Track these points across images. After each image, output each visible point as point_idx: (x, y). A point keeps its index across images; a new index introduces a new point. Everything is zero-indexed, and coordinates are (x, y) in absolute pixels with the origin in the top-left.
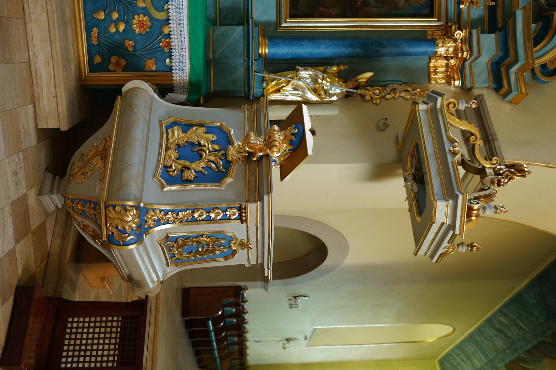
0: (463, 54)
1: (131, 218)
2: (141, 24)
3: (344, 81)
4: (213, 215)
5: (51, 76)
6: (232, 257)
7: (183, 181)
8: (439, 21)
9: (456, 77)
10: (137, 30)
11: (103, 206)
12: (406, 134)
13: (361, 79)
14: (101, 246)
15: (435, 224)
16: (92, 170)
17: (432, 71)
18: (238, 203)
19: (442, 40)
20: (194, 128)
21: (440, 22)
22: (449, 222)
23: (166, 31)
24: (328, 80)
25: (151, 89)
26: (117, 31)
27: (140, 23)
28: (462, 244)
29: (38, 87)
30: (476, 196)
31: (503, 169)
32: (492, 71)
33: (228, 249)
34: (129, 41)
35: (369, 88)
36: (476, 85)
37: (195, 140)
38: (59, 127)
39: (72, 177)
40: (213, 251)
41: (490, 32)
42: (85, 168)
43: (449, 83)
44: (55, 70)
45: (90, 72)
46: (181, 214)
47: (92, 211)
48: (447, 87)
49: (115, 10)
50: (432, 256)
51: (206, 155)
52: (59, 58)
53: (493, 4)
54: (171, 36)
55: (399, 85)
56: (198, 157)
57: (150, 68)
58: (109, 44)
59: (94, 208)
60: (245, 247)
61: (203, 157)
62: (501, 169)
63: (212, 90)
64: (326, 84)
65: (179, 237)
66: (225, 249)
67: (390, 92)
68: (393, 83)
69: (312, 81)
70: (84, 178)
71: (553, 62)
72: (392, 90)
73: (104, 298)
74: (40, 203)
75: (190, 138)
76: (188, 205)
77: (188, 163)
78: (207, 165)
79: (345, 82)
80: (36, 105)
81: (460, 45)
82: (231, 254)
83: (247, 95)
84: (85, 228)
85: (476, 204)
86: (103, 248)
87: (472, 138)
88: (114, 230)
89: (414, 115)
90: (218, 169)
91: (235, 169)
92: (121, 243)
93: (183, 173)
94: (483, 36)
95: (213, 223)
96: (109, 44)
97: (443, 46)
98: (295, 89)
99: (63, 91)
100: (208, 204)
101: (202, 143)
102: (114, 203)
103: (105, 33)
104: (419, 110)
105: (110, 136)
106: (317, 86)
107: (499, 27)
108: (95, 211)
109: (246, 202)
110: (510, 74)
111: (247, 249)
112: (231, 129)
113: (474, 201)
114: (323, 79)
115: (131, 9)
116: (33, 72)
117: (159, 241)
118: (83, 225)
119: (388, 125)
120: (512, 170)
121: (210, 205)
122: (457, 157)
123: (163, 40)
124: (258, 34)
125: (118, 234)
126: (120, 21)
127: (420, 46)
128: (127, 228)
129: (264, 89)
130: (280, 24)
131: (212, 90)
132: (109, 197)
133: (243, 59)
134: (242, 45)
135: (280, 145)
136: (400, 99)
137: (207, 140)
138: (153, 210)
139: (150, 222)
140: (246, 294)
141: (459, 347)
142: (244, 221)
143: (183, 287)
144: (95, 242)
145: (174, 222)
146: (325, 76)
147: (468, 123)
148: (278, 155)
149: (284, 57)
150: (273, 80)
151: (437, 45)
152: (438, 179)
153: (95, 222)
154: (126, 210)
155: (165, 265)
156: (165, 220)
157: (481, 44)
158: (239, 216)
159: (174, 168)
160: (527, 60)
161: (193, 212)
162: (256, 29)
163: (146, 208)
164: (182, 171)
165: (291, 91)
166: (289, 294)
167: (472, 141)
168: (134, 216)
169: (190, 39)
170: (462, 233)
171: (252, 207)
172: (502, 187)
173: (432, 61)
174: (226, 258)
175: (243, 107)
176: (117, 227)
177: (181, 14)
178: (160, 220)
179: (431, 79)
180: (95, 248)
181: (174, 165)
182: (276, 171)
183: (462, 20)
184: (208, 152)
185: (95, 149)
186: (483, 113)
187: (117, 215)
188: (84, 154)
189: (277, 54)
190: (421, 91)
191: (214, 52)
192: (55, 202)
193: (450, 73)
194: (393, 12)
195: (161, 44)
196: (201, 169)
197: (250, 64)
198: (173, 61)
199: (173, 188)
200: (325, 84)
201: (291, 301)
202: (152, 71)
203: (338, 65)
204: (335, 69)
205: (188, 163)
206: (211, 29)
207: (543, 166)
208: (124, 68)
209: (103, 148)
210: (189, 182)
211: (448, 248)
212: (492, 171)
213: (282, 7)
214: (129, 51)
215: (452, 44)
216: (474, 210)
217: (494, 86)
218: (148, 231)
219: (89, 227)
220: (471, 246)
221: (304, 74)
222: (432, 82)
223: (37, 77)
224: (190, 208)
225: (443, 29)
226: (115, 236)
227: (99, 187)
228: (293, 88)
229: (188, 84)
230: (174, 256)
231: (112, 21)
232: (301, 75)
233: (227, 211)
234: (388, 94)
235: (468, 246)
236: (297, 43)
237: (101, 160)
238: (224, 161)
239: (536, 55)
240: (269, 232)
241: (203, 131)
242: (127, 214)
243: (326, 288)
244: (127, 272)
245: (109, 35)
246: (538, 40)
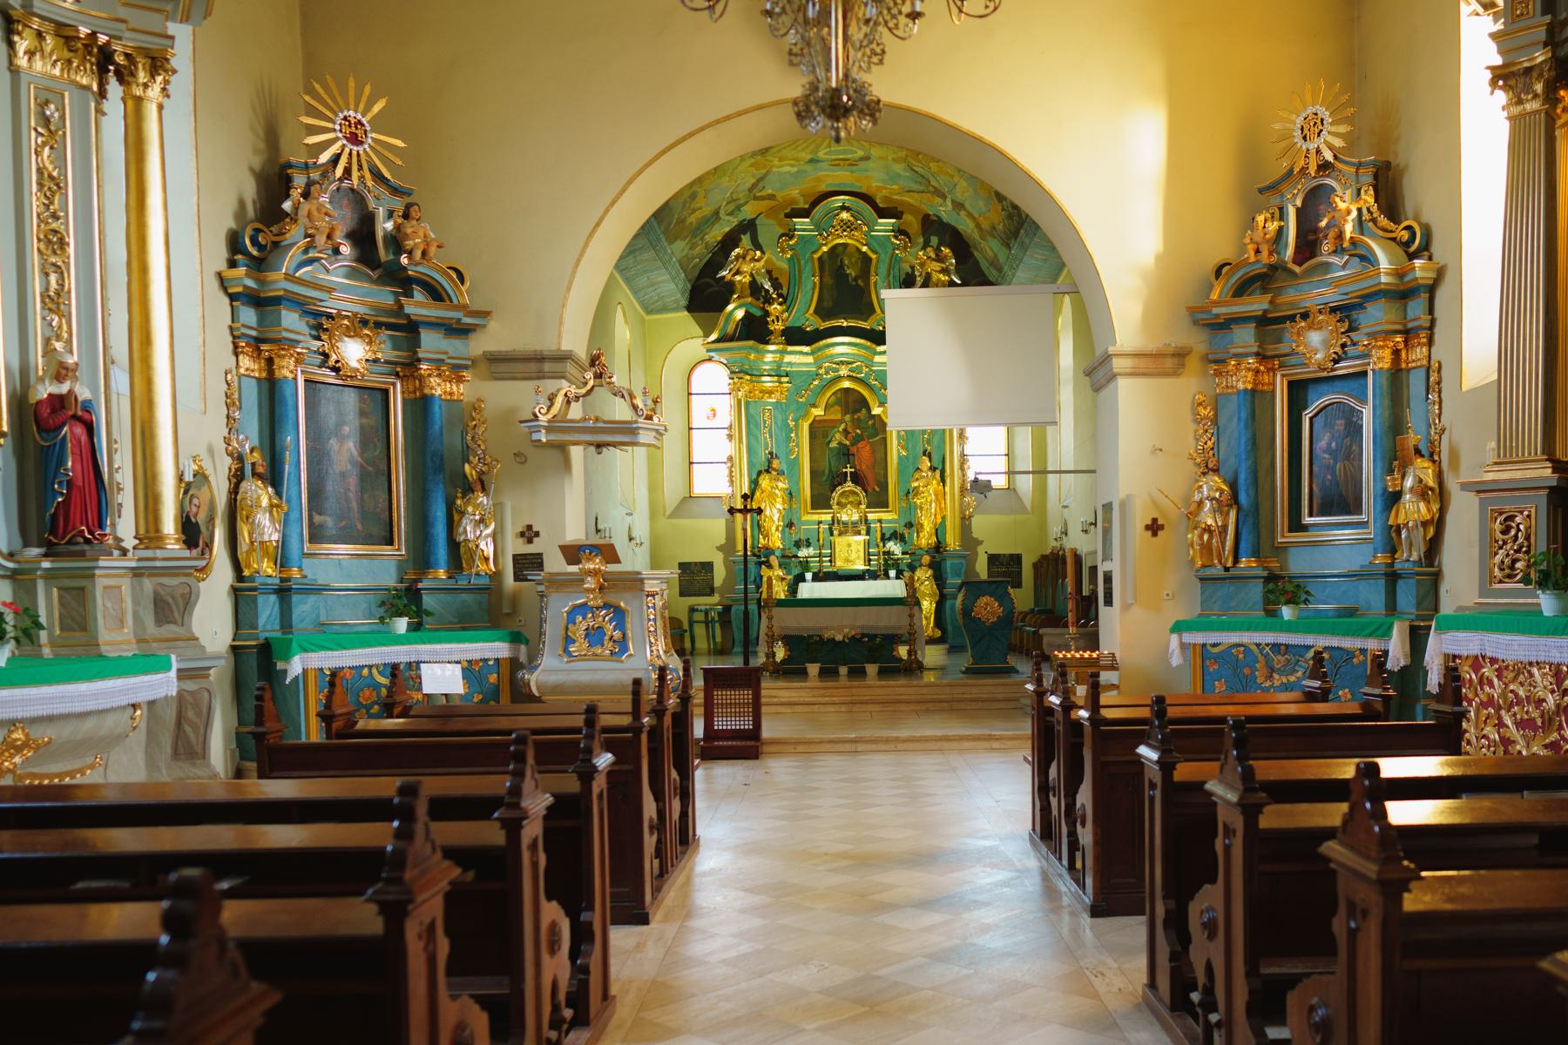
22: (654, 434)
37: (582, 633)
77: (607, 638)
79: (473, 491)
134: (442, 595)
141: (635, 293)
151: (433, 395)
169: (476, 642)
182: (612, 568)
205: (607, 638)
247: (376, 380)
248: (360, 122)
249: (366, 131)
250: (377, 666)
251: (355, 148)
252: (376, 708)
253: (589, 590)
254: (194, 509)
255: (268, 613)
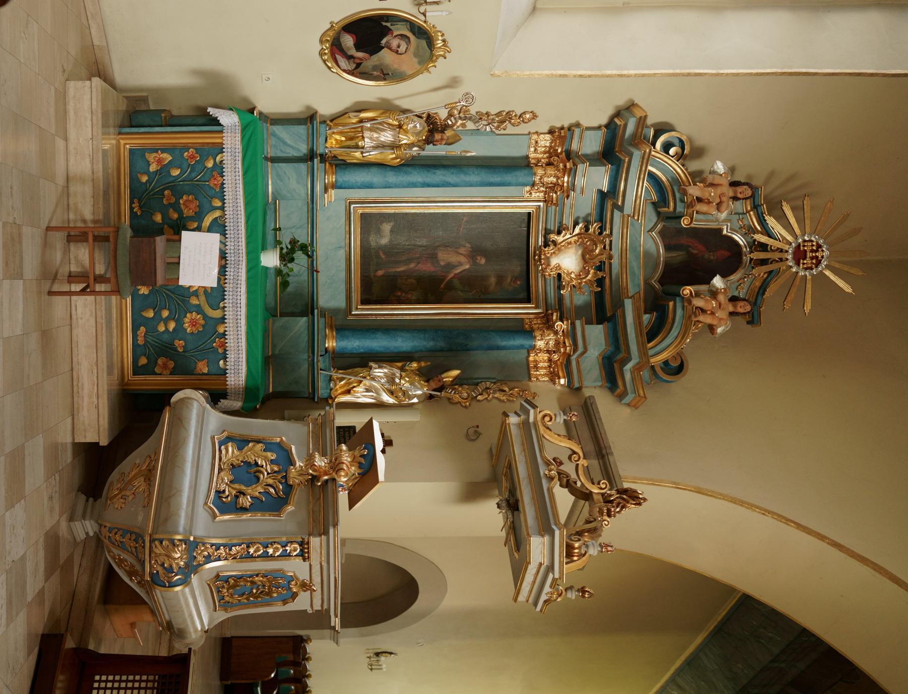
0: (566, 349)
1: (179, 555)
2: (194, 323)
3: (426, 379)
4: (271, 551)
5: (94, 384)
6: (292, 601)
7: (237, 509)
8: (536, 308)
9: (561, 374)
10: (189, 329)
11: (147, 539)
12: (499, 449)
13: (445, 378)
14: (138, 584)
15: (530, 564)
16: (133, 493)
17: (532, 366)
18: (300, 537)
19: (540, 332)
20: (251, 445)
21: (539, 309)
22: (546, 562)
23: (221, 330)
24: (407, 379)
25: (204, 399)
26: (167, 329)
27: (192, 322)
28: (571, 588)
29: (78, 397)
30: (578, 530)
31: (613, 495)
32: (604, 367)
33: (287, 590)
34: (180, 341)
35: (457, 387)
36: (586, 383)
37: (251, 459)
38: (98, 441)
39: (110, 501)
40: (269, 594)
41: (599, 322)
42: (126, 490)
43: (552, 381)
44: (99, 378)
45: (133, 375)
46: (234, 549)
47: (133, 543)
48: (551, 385)
49: (166, 308)
50: (536, 604)
51: (263, 477)
52: (104, 366)
53: (598, 290)
54: (226, 337)
55: (493, 383)
56: (255, 480)
57: (201, 371)
58: (156, 344)
59: (136, 541)
60: (308, 589)
61: (261, 480)
62: (611, 496)
63: (271, 390)
64: (405, 384)
65: (231, 577)
66: (283, 591)
67: (482, 392)
68: (486, 381)
69: (388, 382)
70: (124, 503)
71: (675, 358)
72: (484, 389)
73: (129, 651)
74: (70, 530)
75: (246, 457)
76: (243, 539)
77: (243, 488)
78: (265, 490)
79: (427, 381)
80: (75, 417)
81: (562, 338)
82: (290, 596)
83: (311, 396)
84: (120, 562)
85: (577, 541)
86: (140, 587)
87: (575, 457)
88: (160, 569)
89: (504, 430)
90: (277, 495)
91: (297, 495)
92: (167, 584)
93: (238, 500)
94: (588, 328)
95: (271, 560)
96: (156, 344)
97: (542, 339)
98: (368, 390)
99: (106, 401)
100: (265, 538)
101: (259, 463)
102: (161, 537)
103: (153, 333)
104: (509, 423)
105: (157, 453)
106: (393, 387)
107: (609, 315)
108: (136, 544)
109: (310, 535)
110: (624, 372)
111: (309, 591)
112: (292, 446)
113: (575, 537)
114: (401, 378)
115: (183, 307)
116: (74, 380)
117: (208, 581)
118: (119, 559)
119: (480, 434)
120: (625, 497)
121: (268, 538)
122: (553, 482)
123: (217, 340)
124: (324, 326)
125: (164, 573)
126: (171, 319)
127: (514, 339)
128: (174, 565)
129: (331, 390)
130: (350, 312)
131: (271, 390)
132: (155, 530)
133: (307, 355)
135: (348, 467)
136: (495, 401)
137: (266, 458)
138: (204, 544)
139: (200, 559)
140: (310, 648)
142: (306, 559)
143: (224, 636)
144: (131, 580)
145: (226, 559)
146: (403, 374)
147: (568, 439)
148: (346, 479)
149: (355, 352)
150: (341, 379)
152: (533, 509)
153: (136, 556)
154: (174, 545)
155: (212, 610)
156: (216, 556)
157: (587, 337)
158: (301, 553)
159: (227, 493)
160: (640, 357)
161: (248, 547)
162: (322, 320)
163: (196, 542)
164: (237, 497)
165: (363, 392)
166: (368, 649)
167: (575, 461)
168: (183, 552)
170: (562, 576)
171: (315, 542)
172: (613, 517)
173: (531, 355)
174: (285, 602)
175: (306, 419)
176: (163, 565)
177: (239, 313)
178: (211, 556)
179: (531, 376)
180: (127, 584)
181: (227, 489)
182: (343, 497)
183: (564, 306)
184: (266, 474)
185: (138, 469)
186: (594, 420)
187: (164, 550)
188: (124, 473)
189: (346, 348)
190: (520, 391)
191: (274, 346)
192: (86, 529)
193: (554, 368)
194: (482, 297)
195: (214, 344)
196: (257, 494)
197: (315, 360)
198: (227, 363)
199: (227, 517)
200: (403, 384)
201: (372, 659)
202: (204, 374)
203: (418, 360)
204: (415, 365)
205: (243, 488)
206: (271, 322)
207: (672, 487)
208: (172, 370)
209: (147, 467)
210: (244, 510)
211: (551, 594)
212: (600, 497)
213: (352, 293)
214: (179, 352)
215: (552, 336)
216: (574, 548)
217: (608, 385)
218: (197, 569)
219: (126, 561)
220: (583, 591)
221: (378, 372)
222: (533, 379)
223: (78, 386)
224: (245, 542)
225: (543, 317)
226: (160, 576)
227: (142, 515)
228: (366, 389)
229: (244, 389)
230: (223, 599)
231: (162, 319)
232: (375, 374)
233: (286, 545)
234: (480, 394)
235: (578, 591)
236: (370, 336)
237: (144, 481)
238: (284, 484)
239: (651, 352)
240: (335, 573)
241: (260, 448)
242: (175, 550)
243: (419, 641)
244: (167, 617)
245: (158, 334)
246: (653, 333)
247: (537, 286)
248: (819, 263)
249: (811, 269)
250: (223, 216)
251: (790, 257)
252: (176, 216)
253: (310, 459)
254: (395, 43)
255: (289, 142)
